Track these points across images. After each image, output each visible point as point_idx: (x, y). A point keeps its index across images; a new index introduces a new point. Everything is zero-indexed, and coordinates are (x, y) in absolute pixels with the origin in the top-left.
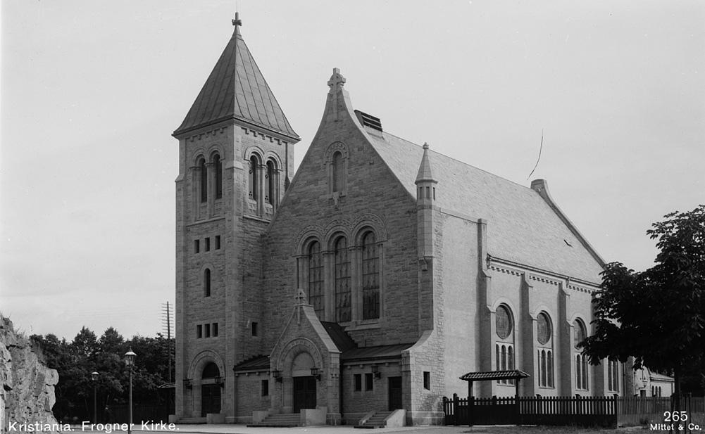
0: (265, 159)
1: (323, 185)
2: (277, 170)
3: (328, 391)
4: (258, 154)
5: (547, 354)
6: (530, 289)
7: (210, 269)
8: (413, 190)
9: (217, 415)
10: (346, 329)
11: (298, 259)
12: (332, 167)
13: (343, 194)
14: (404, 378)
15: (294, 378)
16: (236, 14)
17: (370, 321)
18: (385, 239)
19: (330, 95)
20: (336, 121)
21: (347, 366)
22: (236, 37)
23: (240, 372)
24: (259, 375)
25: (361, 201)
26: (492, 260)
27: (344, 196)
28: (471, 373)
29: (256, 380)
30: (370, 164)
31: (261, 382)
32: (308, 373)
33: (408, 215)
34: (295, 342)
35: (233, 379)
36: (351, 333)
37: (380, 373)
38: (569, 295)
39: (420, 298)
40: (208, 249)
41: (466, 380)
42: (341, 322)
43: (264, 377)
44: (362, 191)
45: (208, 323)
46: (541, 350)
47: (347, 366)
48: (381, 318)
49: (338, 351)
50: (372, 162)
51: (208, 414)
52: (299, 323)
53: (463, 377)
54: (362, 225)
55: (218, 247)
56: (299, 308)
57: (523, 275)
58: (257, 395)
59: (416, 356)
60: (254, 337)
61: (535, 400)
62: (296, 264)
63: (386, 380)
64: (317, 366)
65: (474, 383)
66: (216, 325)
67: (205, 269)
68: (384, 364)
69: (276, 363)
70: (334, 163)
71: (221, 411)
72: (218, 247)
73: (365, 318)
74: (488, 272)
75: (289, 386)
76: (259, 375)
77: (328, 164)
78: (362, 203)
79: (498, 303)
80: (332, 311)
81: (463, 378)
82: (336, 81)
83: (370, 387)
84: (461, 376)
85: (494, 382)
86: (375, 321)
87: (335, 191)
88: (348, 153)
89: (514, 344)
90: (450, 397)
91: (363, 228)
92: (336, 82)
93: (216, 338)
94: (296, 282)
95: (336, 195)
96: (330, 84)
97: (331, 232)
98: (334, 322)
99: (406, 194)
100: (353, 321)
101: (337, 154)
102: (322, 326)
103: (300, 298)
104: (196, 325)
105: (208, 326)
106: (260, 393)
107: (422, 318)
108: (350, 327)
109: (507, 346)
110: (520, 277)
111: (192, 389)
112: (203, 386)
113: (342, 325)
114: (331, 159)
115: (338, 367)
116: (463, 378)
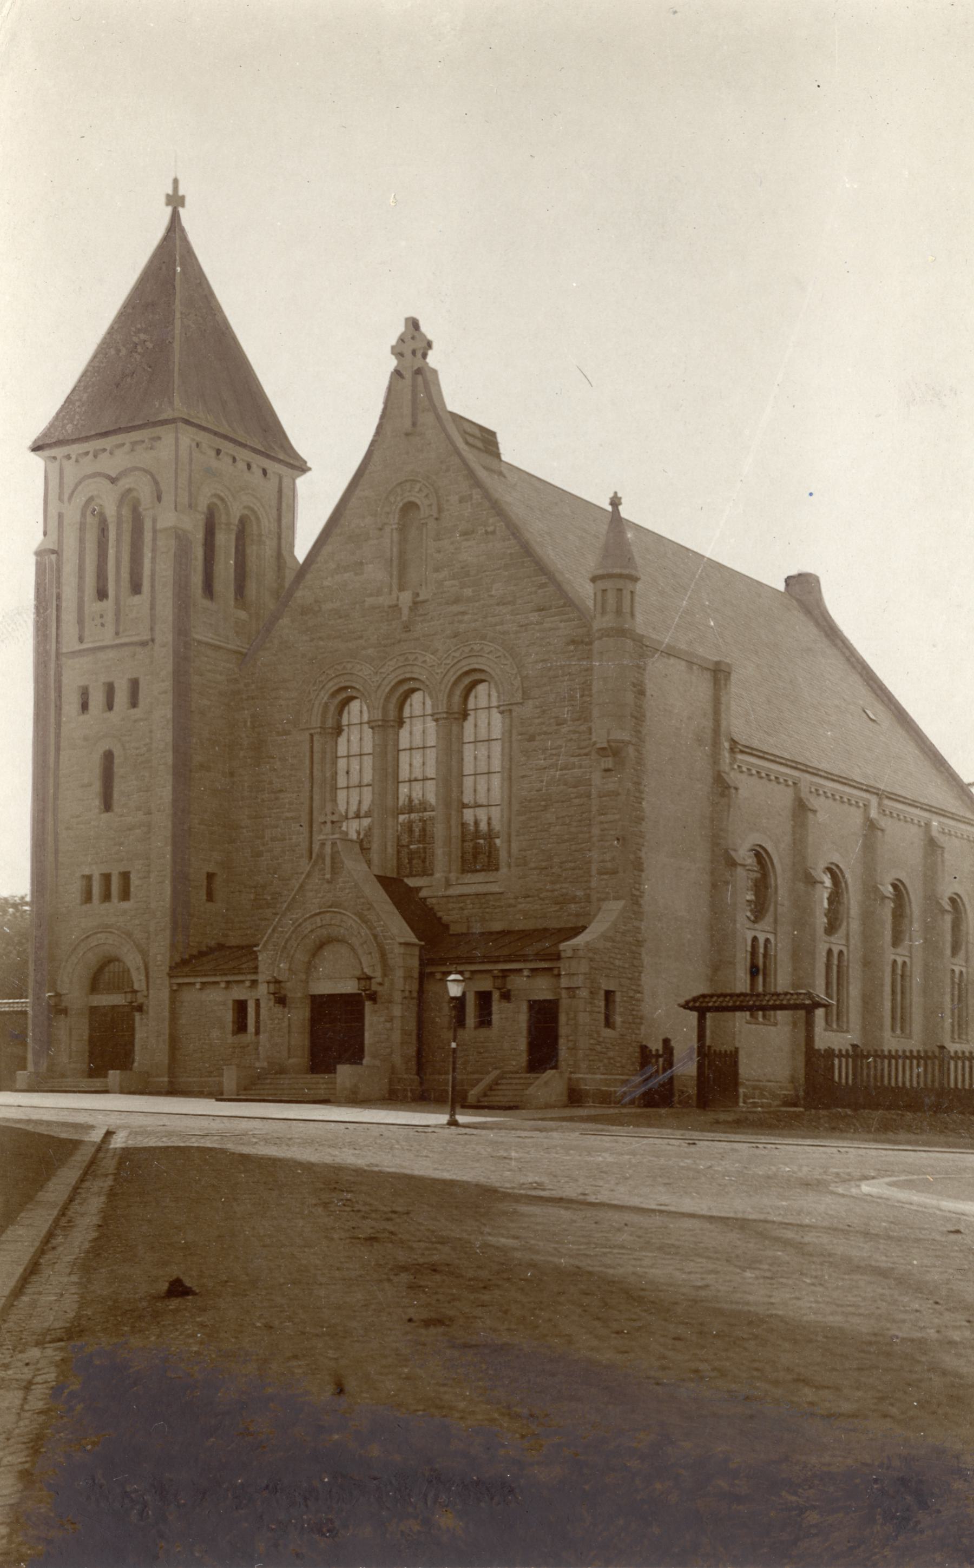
0: (236, 511)
1: (375, 573)
2: (260, 535)
3: (384, 1029)
4: (222, 500)
5: (836, 955)
6: (810, 815)
7: (116, 754)
8: (585, 591)
9: (359, 1066)
10: (423, 894)
11: (312, 735)
12: (395, 534)
13: (421, 598)
14: (565, 1002)
15: (314, 998)
16: (176, 181)
17: (480, 877)
18: (518, 697)
19: (397, 373)
20: (407, 434)
21: (432, 974)
22: (175, 224)
23: (204, 980)
24: (226, 988)
25: (464, 613)
26: (742, 752)
27: (424, 602)
28: (704, 996)
29: (216, 1000)
30: (487, 533)
31: (230, 1004)
32: (349, 987)
33: (572, 648)
34: (318, 919)
35: (165, 994)
36: (434, 901)
37: (509, 991)
38: (883, 830)
39: (596, 831)
40: (110, 706)
41: (691, 1009)
42: (411, 875)
43: (239, 993)
44: (468, 592)
45: (107, 871)
46: (826, 946)
47: (432, 974)
48: (504, 870)
49: (416, 941)
50: (490, 529)
51: (111, 1072)
52: (328, 876)
53: (687, 1002)
54: (465, 666)
55: (134, 704)
56: (329, 844)
57: (928, 825)
58: (221, 1034)
59: (590, 955)
60: (209, 905)
61: (885, 1057)
62: (306, 747)
63: (524, 1007)
64: (368, 971)
65: (709, 1015)
66: (125, 876)
67: (101, 751)
68: (520, 970)
69: (269, 963)
70: (403, 529)
71: (365, 1061)
72: (134, 704)
73: (463, 871)
74: (733, 777)
75: (300, 1015)
76: (226, 988)
77: (388, 529)
78: (466, 618)
79: (747, 845)
80: (390, 850)
81: (686, 1006)
82: (410, 345)
83: (485, 1020)
84: (682, 1001)
85: (741, 1018)
86: (491, 876)
87: (401, 588)
88: (435, 507)
89: (775, 934)
90: (656, 1046)
91: (467, 673)
92: (413, 345)
93: (125, 905)
94: (307, 785)
95: (406, 598)
96: (397, 352)
97: (393, 679)
98: (395, 876)
99: (568, 603)
100: (438, 875)
101: (410, 507)
102: (378, 885)
103: (333, 822)
104: (78, 875)
105: (107, 878)
106: (230, 1027)
107: (600, 873)
108: (430, 887)
109: (900, 960)
110: (862, 810)
111: (66, 1014)
112: (93, 1010)
113: (412, 882)
114: (394, 520)
115: (416, 975)
116: (686, 1006)
